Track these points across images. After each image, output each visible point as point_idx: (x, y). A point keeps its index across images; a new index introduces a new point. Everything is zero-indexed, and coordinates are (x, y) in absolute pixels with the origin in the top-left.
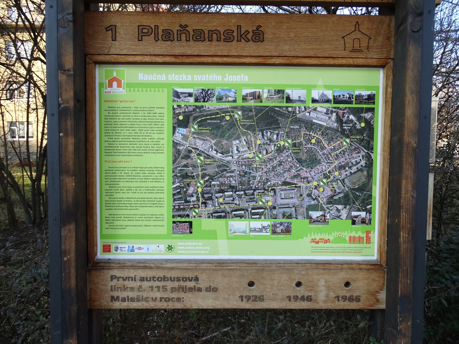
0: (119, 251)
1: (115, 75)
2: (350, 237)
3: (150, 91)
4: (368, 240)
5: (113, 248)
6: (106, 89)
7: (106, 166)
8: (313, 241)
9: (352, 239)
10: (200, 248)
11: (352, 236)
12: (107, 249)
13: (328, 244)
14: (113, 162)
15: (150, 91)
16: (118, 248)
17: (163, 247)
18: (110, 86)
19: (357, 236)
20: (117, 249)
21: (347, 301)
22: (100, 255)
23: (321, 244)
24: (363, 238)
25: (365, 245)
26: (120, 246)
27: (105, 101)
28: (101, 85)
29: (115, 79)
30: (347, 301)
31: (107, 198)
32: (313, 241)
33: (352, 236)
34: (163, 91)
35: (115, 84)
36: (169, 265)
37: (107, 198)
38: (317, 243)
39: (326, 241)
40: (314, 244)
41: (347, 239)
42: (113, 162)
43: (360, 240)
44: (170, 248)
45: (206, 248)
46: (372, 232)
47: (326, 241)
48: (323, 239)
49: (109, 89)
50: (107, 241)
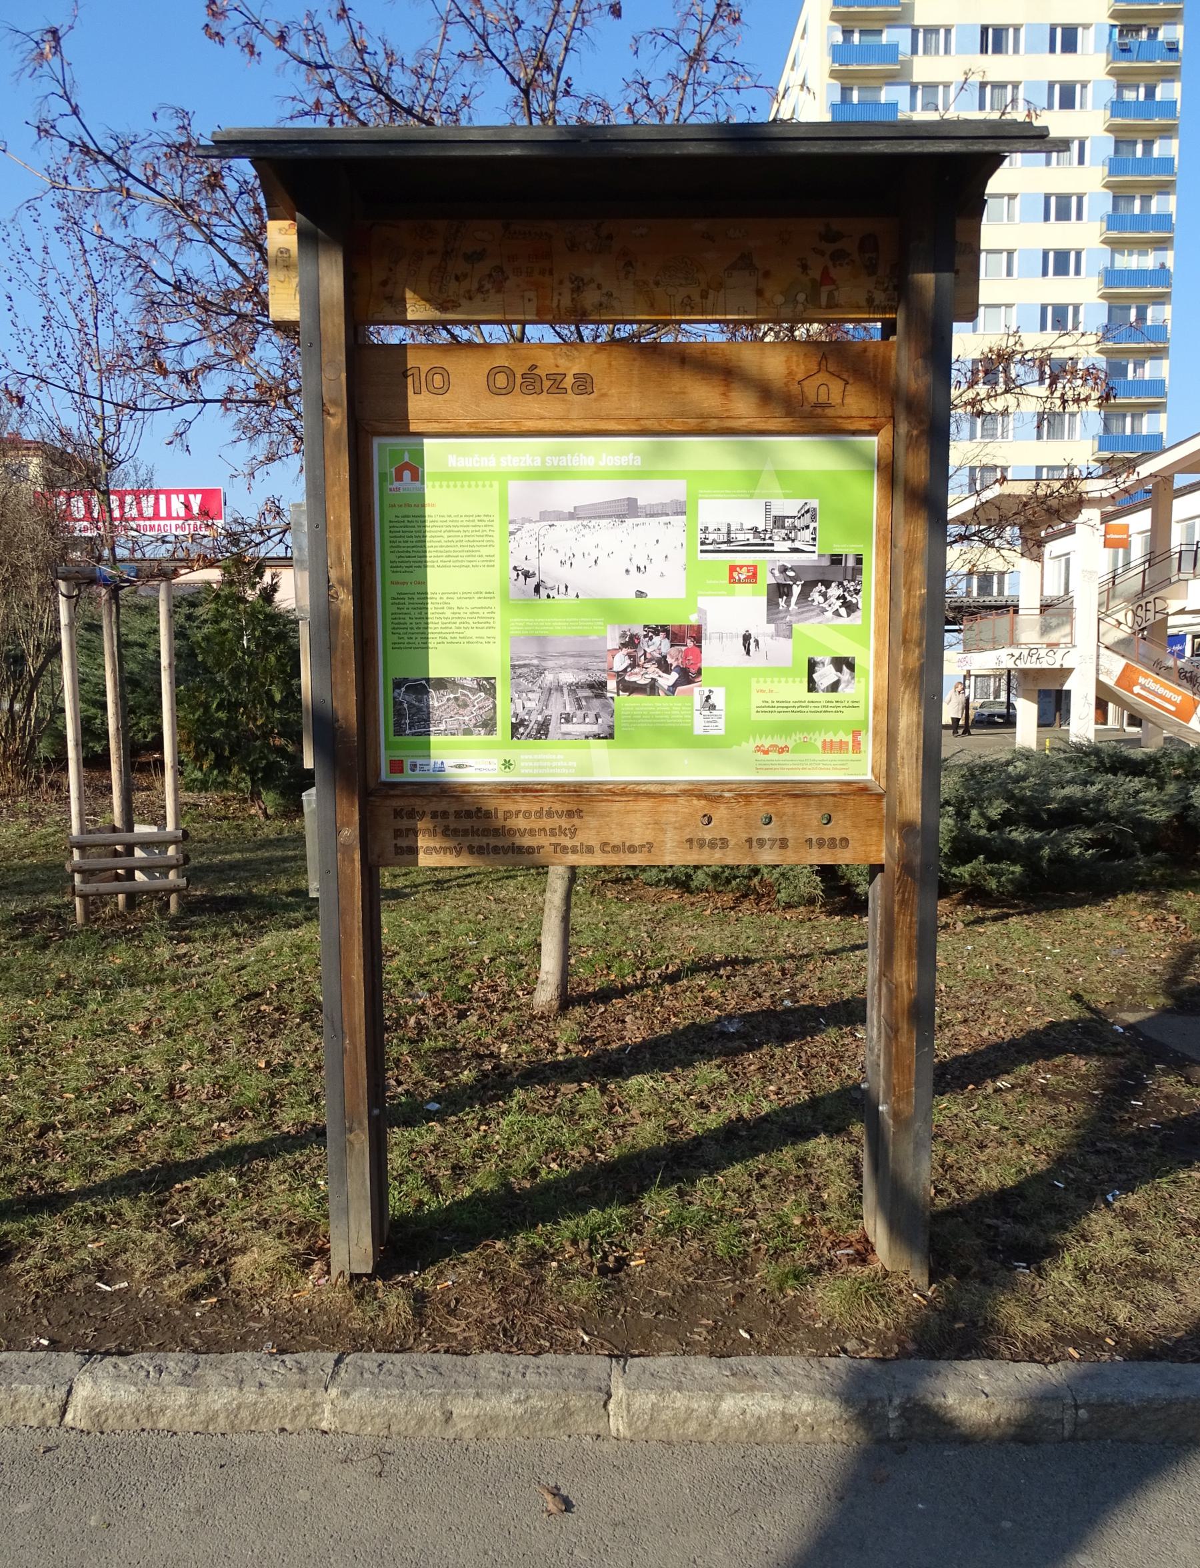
0: (417, 771)
1: (407, 459)
2: (824, 742)
3: (470, 486)
4: (857, 746)
5: (407, 766)
6: (392, 484)
7: (392, 591)
8: (759, 749)
9: (828, 745)
10: (560, 764)
11: (828, 740)
12: (397, 766)
13: (785, 755)
14: (404, 583)
15: (470, 486)
16: (415, 766)
17: (497, 763)
18: (399, 478)
19: (836, 739)
20: (414, 767)
21: (707, 848)
22: (385, 775)
23: (773, 756)
24: (847, 743)
25: (850, 756)
26: (419, 761)
27: (392, 583)
28: (383, 477)
29: (407, 466)
30: (707, 848)
31: (393, 557)
32: (759, 749)
33: (828, 740)
34: (491, 486)
35: (407, 474)
36: (539, 787)
37: (393, 557)
38: (766, 752)
39: (782, 750)
40: (760, 756)
41: (819, 744)
42: (404, 583)
43: (842, 746)
44: (507, 764)
45: (570, 764)
46: (863, 733)
47: (782, 750)
48: (776, 746)
49: (397, 484)
50: (398, 754)
